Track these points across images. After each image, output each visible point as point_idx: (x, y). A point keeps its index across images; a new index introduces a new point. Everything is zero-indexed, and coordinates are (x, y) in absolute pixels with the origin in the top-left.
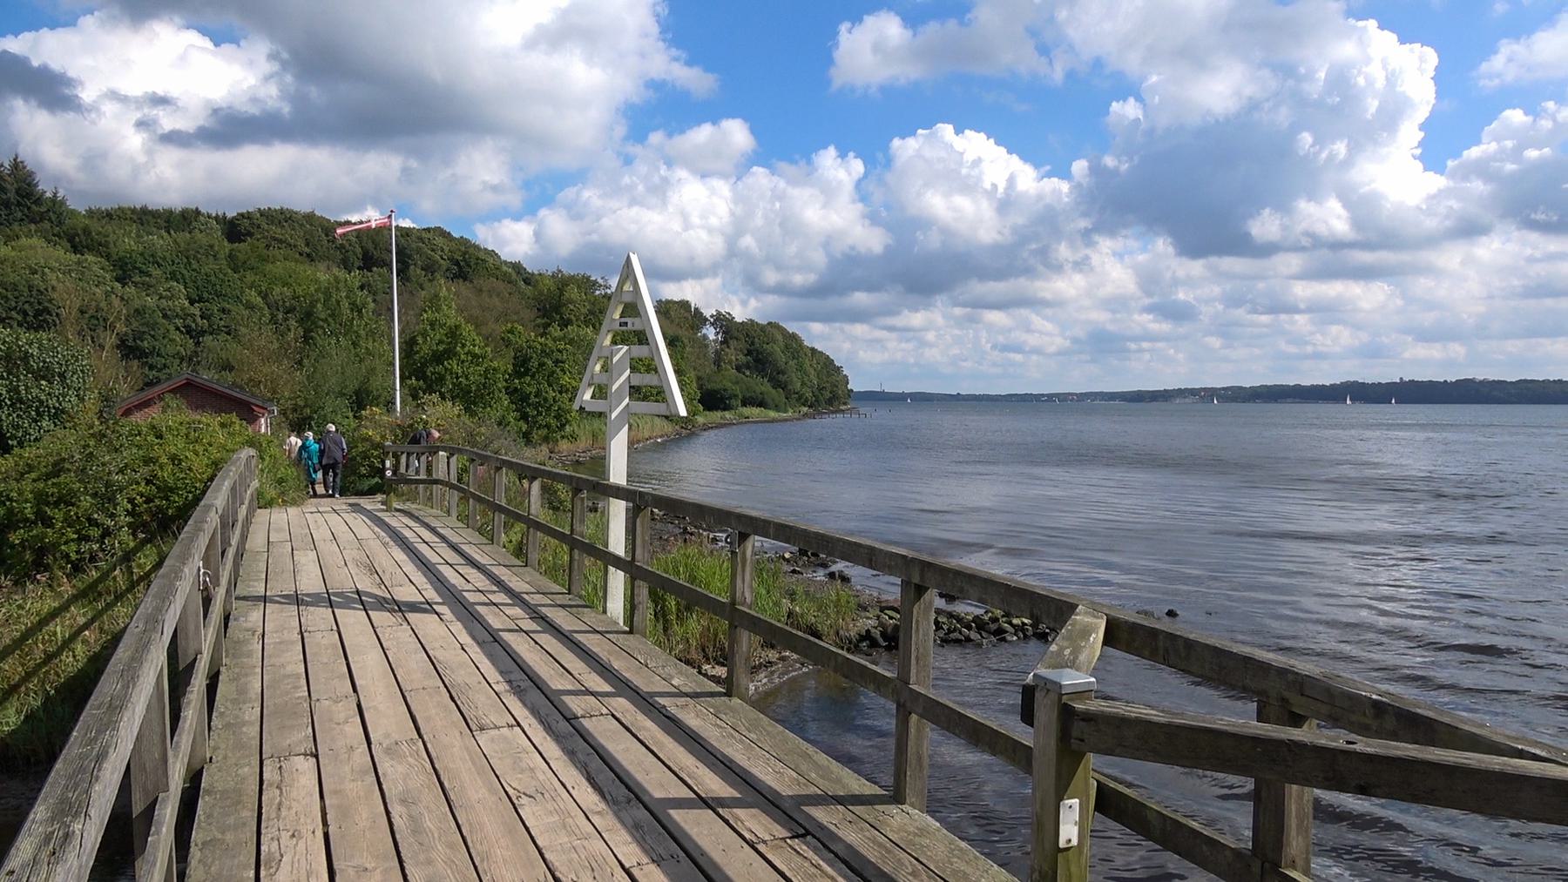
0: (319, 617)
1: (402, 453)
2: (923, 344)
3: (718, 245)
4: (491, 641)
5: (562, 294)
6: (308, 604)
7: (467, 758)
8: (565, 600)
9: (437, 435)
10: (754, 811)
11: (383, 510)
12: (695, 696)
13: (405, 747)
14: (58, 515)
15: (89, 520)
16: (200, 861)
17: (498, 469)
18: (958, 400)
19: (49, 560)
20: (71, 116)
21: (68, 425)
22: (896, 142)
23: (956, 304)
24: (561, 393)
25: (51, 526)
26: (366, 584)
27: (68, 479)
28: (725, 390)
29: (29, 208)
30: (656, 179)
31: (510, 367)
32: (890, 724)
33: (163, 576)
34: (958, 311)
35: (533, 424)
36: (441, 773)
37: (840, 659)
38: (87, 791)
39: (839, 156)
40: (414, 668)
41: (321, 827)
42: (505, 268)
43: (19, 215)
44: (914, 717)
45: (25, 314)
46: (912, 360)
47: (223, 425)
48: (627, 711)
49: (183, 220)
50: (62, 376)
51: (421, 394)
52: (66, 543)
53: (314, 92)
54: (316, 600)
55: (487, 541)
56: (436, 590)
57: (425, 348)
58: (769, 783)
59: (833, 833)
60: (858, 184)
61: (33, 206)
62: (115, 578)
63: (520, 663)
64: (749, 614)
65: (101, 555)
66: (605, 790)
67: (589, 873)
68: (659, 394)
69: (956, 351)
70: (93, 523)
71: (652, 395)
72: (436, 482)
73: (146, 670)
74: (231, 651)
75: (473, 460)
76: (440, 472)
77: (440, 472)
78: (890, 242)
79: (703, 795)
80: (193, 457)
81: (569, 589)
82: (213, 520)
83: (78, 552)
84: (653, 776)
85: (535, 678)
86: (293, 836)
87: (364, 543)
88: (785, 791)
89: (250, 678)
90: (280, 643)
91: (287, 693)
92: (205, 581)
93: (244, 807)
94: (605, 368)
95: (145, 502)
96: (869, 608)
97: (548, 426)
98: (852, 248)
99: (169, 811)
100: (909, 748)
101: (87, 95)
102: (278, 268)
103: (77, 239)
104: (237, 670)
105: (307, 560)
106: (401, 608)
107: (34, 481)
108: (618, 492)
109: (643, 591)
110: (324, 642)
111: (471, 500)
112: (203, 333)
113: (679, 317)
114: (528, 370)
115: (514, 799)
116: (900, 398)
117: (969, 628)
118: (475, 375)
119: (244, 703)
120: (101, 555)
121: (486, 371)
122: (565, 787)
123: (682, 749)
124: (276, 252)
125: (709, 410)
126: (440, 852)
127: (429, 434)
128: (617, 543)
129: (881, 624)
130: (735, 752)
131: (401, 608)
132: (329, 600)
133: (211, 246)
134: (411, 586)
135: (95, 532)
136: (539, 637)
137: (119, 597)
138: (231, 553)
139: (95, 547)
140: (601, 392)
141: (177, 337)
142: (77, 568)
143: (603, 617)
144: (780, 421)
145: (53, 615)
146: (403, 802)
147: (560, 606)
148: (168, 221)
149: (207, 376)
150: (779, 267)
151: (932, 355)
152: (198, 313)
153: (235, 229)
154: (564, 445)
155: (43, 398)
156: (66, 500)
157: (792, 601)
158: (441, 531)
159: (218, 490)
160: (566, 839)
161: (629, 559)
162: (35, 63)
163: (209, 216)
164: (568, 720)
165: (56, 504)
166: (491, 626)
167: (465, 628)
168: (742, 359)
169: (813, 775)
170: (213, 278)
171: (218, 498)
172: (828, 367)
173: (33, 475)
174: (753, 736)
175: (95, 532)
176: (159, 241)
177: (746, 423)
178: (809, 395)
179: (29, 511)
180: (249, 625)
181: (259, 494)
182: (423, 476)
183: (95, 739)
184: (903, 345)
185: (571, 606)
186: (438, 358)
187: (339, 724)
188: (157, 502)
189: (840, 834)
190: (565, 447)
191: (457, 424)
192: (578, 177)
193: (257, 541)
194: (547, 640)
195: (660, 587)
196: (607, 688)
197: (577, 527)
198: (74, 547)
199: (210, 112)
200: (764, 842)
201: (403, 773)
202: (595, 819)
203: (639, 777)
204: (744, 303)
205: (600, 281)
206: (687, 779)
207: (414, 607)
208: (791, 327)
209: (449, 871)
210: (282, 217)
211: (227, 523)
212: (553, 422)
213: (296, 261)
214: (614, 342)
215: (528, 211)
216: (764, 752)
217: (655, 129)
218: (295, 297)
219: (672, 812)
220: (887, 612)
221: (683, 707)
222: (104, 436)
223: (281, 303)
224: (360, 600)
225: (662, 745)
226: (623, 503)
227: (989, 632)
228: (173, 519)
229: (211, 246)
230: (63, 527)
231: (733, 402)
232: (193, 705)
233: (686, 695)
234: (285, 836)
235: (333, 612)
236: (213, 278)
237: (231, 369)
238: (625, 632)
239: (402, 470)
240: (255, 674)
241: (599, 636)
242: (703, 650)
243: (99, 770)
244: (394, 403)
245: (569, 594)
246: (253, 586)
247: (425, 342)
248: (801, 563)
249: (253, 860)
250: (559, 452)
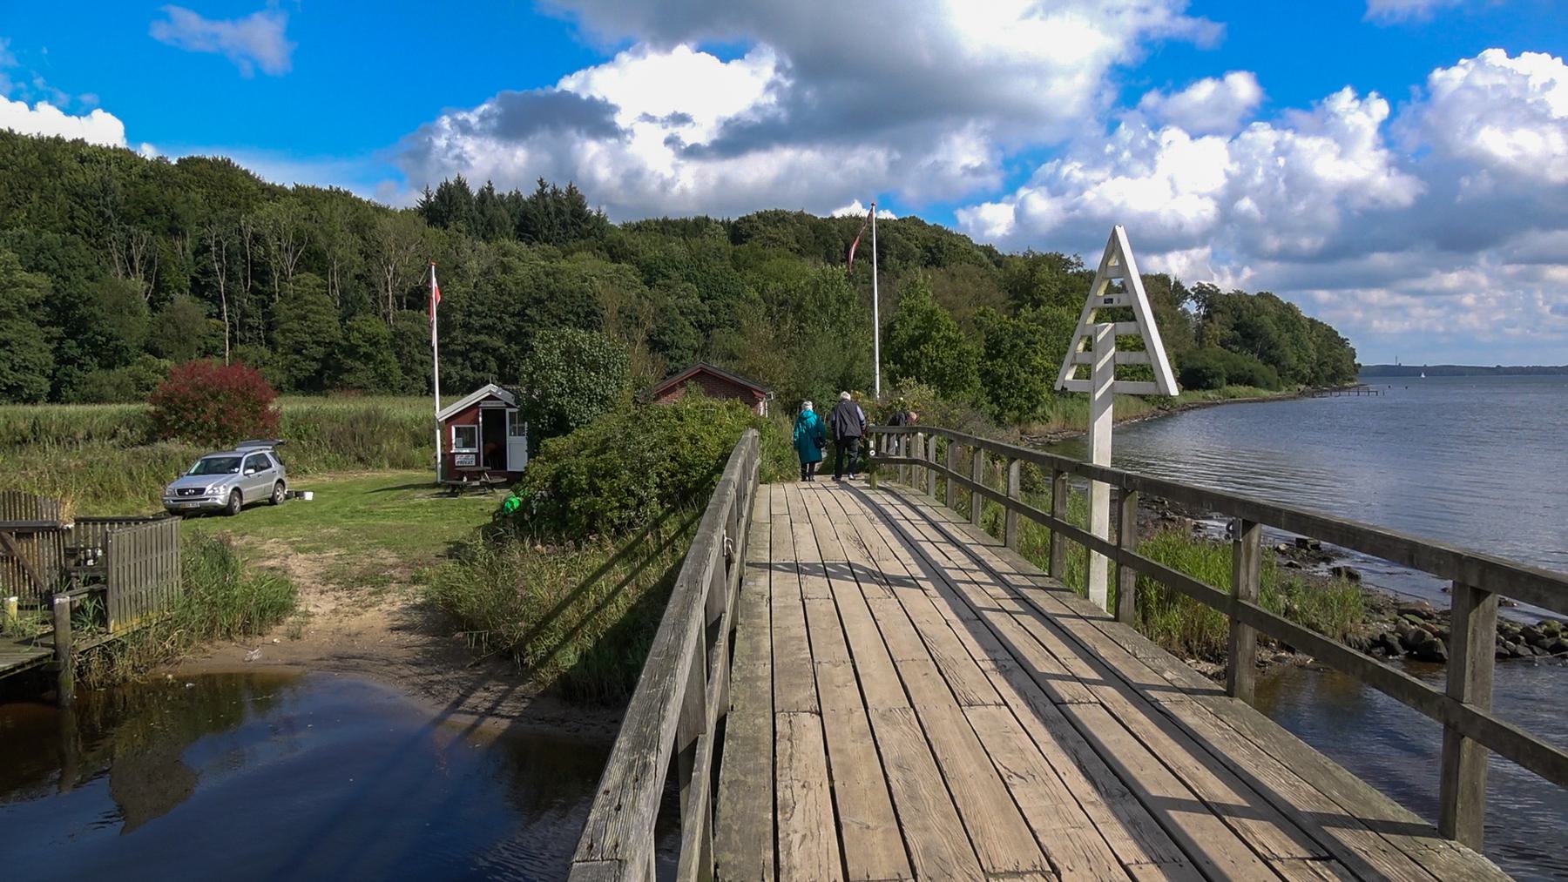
0: (816, 585)
1: (884, 434)
2: (1459, 308)
3: (1209, 210)
4: (975, 619)
5: (1033, 275)
6: (807, 573)
7: (957, 731)
8: (1046, 582)
9: (915, 416)
10: (1265, 823)
11: (867, 488)
12: (1190, 692)
13: (898, 714)
14: (604, 485)
15: (628, 490)
16: (727, 798)
17: (977, 450)
18: (1499, 374)
19: (599, 523)
20: (612, 141)
21: (610, 409)
22: (1438, 74)
23: (1509, 262)
24: (1032, 374)
25: (600, 495)
26: (856, 557)
27: (613, 455)
28: (1207, 368)
29: (580, 226)
30: (1143, 143)
31: (982, 350)
32: (1437, 743)
33: (698, 543)
34: (1510, 269)
35: (1005, 406)
36: (933, 742)
37: (1370, 666)
38: (657, 727)
39: (1356, 98)
40: (903, 640)
41: (827, 781)
42: (976, 252)
43: (573, 233)
44: (1468, 742)
45: (578, 315)
46: (1441, 329)
47: (729, 408)
48: (1117, 701)
49: (696, 228)
50: (606, 367)
51: (899, 378)
52: (610, 510)
53: (809, 94)
54: (813, 570)
55: (965, 521)
56: (920, 566)
57: (902, 334)
58: (1282, 795)
59: (1363, 860)
60: (1384, 127)
61: (583, 225)
62: (647, 541)
63: (1004, 642)
64: (1254, 609)
65: (637, 521)
66: (1097, 780)
67: (1085, 862)
68: (1147, 372)
69: (1501, 316)
70: (631, 493)
71: (1126, 375)
72: (916, 462)
73: (692, 624)
74: (744, 612)
75: (952, 441)
76: (919, 454)
77: (919, 454)
78: (1421, 190)
79: (1206, 800)
80: (707, 437)
81: (1050, 572)
82: (732, 491)
83: (619, 518)
84: (1148, 772)
85: (1020, 659)
86: (804, 786)
87: (852, 518)
88: (1303, 807)
89: (762, 637)
90: (785, 607)
91: (793, 654)
92: (728, 548)
93: (761, 754)
94: (1088, 348)
95: (670, 476)
96: (1385, 611)
97: (1019, 408)
98: (1375, 201)
99: (707, 747)
100: (1460, 776)
101: (621, 121)
102: (772, 266)
103: (614, 250)
104: (750, 629)
105: (803, 531)
106: (889, 581)
107: (588, 457)
108: (1102, 475)
109: (1130, 580)
110: (823, 609)
111: (949, 480)
112: (712, 326)
113: (1164, 291)
114: (999, 352)
115: (1005, 777)
116: (1413, 372)
117: (1516, 640)
118: (949, 357)
119: (758, 660)
120: (637, 521)
121: (960, 354)
122: (1056, 773)
123: (1179, 747)
124: (771, 251)
125: (1189, 389)
126: (935, 820)
127: (908, 416)
128: (1101, 526)
129: (1400, 629)
130: (1240, 756)
131: (889, 581)
132: (825, 570)
133: (719, 249)
134: (898, 562)
135: (632, 502)
136: (1021, 618)
137: (650, 559)
138: (743, 522)
139: (633, 514)
140: (1085, 372)
141: (691, 330)
142: (619, 532)
143: (1084, 602)
144: (1271, 400)
145: (603, 570)
146: (899, 767)
147: (1042, 588)
148: (684, 230)
149: (716, 365)
150: (1279, 232)
151: (1470, 321)
152: (707, 309)
153: (738, 232)
154: (1036, 427)
155: (592, 387)
156: (610, 474)
157: (1289, 595)
158: (923, 509)
159: (733, 467)
160: (1059, 825)
161: (1114, 543)
162: (584, 97)
163: (716, 222)
164: (1055, 704)
165: (604, 477)
166: (973, 605)
167: (949, 604)
168: (1228, 333)
169: (1336, 793)
170: (720, 278)
171: (733, 473)
172: (1331, 340)
173: (587, 452)
174: (1260, 742)
175: (632, 502)
176: (678, 248)
177: (1232, 403)
178: (1307, 371)
179: (584, 484)
180: (758, 589)
181: (761, 471)
182: (904, 457)
183: (659, 683)
184: (1432, 312)
185: (1052, 589)
186: (914, 343)
187: (838, 687)
188: (679, 476)
189: (1372, 862)
190: (1036, 429)
191: (932, 406)
192: (1059, 151)
193: (761, 513)
194: (1029, 621)
195: (1147, 570)
196: (1094, 675)
197: (1058, 510)
198: (616, 513)
199: (722, 125)
200: (1280, 860)
201: (898, 739)
202: (1088, 808)
203: (1134, 771)
204: (1236, 273)
205: (1073, 259)
206: (1186, 779)
207: (900, 581)
208: (1284, 298)
209: (945, 841)
210: (777, 219)
211: (740, 497)
212: (1025, 404)
213: (787, 257)
214: (1098, 320)
215: (1007, 191)
216: (1274, 761)
217: (1148, 89)
218: (787, 291)
219: (1171, 812)
220: (1407, 616)
221: (1177, 703)
222: (639, 418)
223: (775, 297)
224: (852, 572)
225: (1157, 742)
226: (1107, 486)
227: (1544, 648)
228: (692, 491)
229: (719, 249)
230: (608, 497)
231: (1217, 382)
232: (721, 657)
233: (1181, 690)
234: (797, 785)
235: (829, 582)
236: (720, 278)
237: (735, 358)
238: (1109, 619)
239: (884, 450)
240: (765, 634)
241: (1083, 622)
242: (1187, 643)
243: (664, 711)
244: (874, 387)
245: (1050, 576)
246: (760, 554)
247: (902, 328)
248: (1298, 556)
249: (771, 803)
250: (1031, 433)
